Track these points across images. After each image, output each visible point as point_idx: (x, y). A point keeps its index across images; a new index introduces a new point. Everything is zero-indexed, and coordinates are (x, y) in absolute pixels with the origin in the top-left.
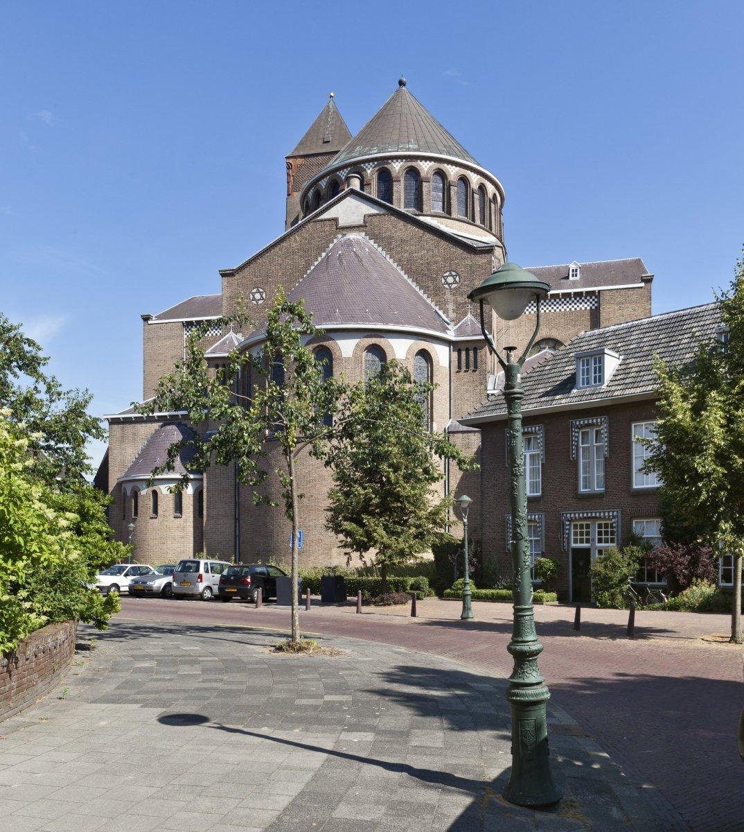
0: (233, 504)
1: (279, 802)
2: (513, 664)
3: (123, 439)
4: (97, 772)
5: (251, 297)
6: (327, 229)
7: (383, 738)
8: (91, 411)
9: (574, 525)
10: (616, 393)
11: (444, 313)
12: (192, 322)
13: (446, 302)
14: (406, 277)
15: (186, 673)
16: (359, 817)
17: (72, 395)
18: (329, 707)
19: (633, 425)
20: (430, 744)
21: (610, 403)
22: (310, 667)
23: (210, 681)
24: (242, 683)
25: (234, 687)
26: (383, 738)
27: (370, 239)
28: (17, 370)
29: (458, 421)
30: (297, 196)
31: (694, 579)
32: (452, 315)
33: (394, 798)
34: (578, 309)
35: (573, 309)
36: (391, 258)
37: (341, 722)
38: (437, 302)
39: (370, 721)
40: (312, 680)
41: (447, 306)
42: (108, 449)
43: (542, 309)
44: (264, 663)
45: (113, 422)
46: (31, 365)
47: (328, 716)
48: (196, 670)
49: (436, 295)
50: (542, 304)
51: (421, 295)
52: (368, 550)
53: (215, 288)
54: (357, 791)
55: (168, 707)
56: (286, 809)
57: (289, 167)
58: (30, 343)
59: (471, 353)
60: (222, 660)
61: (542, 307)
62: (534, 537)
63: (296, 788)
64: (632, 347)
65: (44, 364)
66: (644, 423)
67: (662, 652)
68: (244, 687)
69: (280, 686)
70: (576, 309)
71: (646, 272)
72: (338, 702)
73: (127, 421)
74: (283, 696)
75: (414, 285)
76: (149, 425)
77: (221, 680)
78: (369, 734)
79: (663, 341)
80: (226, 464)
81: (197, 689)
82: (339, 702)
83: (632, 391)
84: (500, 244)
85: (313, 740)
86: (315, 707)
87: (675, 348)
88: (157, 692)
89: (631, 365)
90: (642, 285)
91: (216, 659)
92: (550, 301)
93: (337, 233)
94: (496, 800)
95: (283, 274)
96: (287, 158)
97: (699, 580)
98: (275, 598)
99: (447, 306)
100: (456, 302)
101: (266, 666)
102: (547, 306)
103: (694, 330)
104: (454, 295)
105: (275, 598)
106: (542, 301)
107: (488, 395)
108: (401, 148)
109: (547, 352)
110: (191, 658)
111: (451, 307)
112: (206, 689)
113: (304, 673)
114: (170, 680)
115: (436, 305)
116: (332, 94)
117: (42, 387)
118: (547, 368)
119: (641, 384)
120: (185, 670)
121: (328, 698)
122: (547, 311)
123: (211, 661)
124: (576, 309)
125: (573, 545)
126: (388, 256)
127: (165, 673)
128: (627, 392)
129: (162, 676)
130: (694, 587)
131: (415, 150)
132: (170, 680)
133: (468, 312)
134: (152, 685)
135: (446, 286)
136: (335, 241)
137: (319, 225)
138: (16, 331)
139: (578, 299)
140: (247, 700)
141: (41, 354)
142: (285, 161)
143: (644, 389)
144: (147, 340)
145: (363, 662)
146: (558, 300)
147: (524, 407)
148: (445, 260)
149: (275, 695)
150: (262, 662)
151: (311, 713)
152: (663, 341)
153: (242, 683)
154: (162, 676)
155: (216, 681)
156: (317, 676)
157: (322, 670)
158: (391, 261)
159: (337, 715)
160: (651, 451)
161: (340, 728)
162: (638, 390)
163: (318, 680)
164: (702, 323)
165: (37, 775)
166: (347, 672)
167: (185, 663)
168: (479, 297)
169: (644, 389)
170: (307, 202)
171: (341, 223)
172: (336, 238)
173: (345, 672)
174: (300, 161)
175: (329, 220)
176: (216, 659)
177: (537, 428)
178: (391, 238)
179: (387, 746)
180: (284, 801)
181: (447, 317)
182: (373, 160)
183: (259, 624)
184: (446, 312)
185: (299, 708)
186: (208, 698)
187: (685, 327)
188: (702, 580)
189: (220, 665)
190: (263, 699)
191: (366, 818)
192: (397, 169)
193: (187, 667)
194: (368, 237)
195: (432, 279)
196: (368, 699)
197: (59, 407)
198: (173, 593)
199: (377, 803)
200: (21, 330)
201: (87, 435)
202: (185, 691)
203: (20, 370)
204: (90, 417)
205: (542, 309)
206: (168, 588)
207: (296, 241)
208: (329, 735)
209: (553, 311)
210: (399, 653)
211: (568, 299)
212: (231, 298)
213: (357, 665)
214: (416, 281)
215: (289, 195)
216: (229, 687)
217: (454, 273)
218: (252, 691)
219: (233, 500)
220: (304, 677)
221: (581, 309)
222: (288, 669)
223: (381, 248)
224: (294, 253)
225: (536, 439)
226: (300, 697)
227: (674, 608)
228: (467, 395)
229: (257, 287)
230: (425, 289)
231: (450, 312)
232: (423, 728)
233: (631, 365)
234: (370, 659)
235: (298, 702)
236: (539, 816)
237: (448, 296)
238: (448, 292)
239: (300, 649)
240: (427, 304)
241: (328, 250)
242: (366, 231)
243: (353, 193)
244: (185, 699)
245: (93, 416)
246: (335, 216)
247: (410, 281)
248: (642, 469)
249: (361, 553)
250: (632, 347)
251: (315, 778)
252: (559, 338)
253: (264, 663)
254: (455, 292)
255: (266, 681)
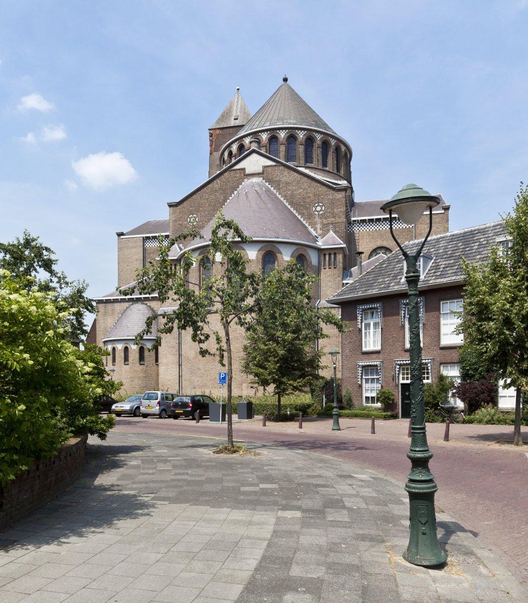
0: (178, 355)
1: (250, 564)
2: (411, 466)
3: (105, 314)
4: (117, 542)
5: (189, 220)
6: (237, 175)
7: (307, 515)
8: (87, 295)
9: (402, 368)
10: (431, 282)
11: (314, 230)
12: (149, 237)
13: (316, 223)
14: (289, 207)
15: (162, 468)
16: (309, 576)
17: (75, 284)
18: (264, 492)
19: (441, 303)
20: (341, 520)
21: (426, 289)
22: (244, 464)
23: (180, 474)
24: (200, 476)
25: (197, 479)
26: (307, 515)
27: (266, 182)
28: (38, 268)
29: (326, 301)
30: (217, 155)
31: (483, 403)
32: (320, 232)
33: (329, 560)
34: (401, 228)
35: (398, 228)
36: (279, 194)
37: (275, 503)
38: (310, 223)
39: (295, 503)
40: (247, 473)
41: (316, 226)
42: (95, 320)
43: (394, 226)
44: (212, 462)
45: (99, 302)
46: (48, 265)
47: (265, 499)
48: (168, 467)
49: (309, 218)
50: (394, 223)
51: (300, 218)
52: (269, 385)
53: (164, 214)
54: (300, 556)
55: (156, 493)
56: (256, 570)
57: (211, 135)
58: (47, 249)
59: (332, 256)
60: (185, 460)
61: (394, 225)
62: (371, 376)
63: (258, 553)
64: (440, 251)
65: (54, 264)
66: (456, 301)
67: (472, 452)
68: (203, 478)
69: (228, 478)
70: (399, 228)
71: (444, 203)
72: (269, 489)
73: (108, 302)
74: (231, 485)
75: (294, 212)
76: (122, 304)
77: (187, 474)
78: (297, 512)
79: (461, 247)
80: (151, 332)
81: (173, 480)
82: (271, 489)
83: (442, 280)
84: (349, 186)
85: (260, 516)
86: (255, 493)
87: (469, 252)
88: (146, 483)
89: (440, 263)
90: (443, 211)
91: (180, 458)
92: (383, 222)
93: (244, 179)
94: (400, 561)
95: (209, 205)
96: (210, 130)
97: (486, 404)
98: (208, 417)
99: (316, 226)
100: (322, 223)
101: (214, 464)
102: (381, 226)
103: (481, 240)
104: (321, 218)
105: (208, 417)
106: (394, 221)
107: (343, 284)
108: (285, 123)
109: (382, 256)
110: (163, 458)
111: (319, 226)
112: (179, 480)
113: (242, 468)
114: (153, 474)
115: (309, 225)
116: (238, 88)
117: (55, 280)
118: (384, 266)
119: (448, 276)
120: (161, 466)
121: (262, 486)
122: (381, 229)
123: (177, 460)
124: (399, 228)
125: (402, 382)
126: (278, 193)
127: (148, 468)
128: (438, 281)
129: (146, 471)
130: (483, 409)
131: (294, 124)
132: (153, 474)
133: (330, 230)
134: (141, 477)
135: (316, 213)
136: (243, 183)
137: (232, 173)
138: (36, 242)
139: (378, 223)
140: (208, 487)
141: (53, 257)
142: (208, 131)
143: (449, 279)
144: (120, 249)
145: (278, 460)
146: (365, 224)
147: (369, 291)
148: (315, 195)
149: (226, 484)
150: (210, 460)
151: (253, 497)
152: (461, 247)
153: (200, 476)
154: (146, 471)
155: (183, 474)
156: (251, 470)
157: (252, 466)
158: (280, 196)
159: (272, 498)
160: (461, 320)
161: (276, 508)
162: (446, 279)
163: (252, 473)
164: (487, 236)
165: (77, 545)
166: (270, 467)
167: (159, 461)
168: (388, 209)
169: (449, 279)
170: (224, 159)
171: (247, 172)
172: (243, 181)
173: (268, 467)
174: (218, 132)
175: (239, 169)
176: (180, 458)
177: (378, 305)
178: (280, 181)
179: (312, 521)
180: (253, 563)
181: (317, 233)
182: (266, 130)
183: (200, 434)
184: (315, 230)
185: (244, 493)
186: (182, 487)
187: (475, 238)
188: (488, 404)
189: (183, 463)
190: (219, 487)
191: (314, 576)
192: (283, 136)
193: (162, 465)
194: (264, 181)
195: (307, 208)
196: (289, 487)
197: (67, 292)
198: (140, 413)
199: (318, 565)
200: (39, 241)
201: (85, 310)
202: (165, 482)
203: (40, 267)
204: (87, 298)
205: (394, 226)
206: (137, 411)
207: (217, 184)
208: (270, 513)
209: (384, 229)
210: (299, 454)
211: (365, 224)
212: (175, 221)
213: (275, 463)
214: (296, 209)
215: (210, 154)
216: (193, 478)
217: (316, 205)
218: (210, 481)
219: (178, 354)
220: (242, 471)
221: (403, 227)
222: (228, 466)
223: (273, 188)
224: (216, 191)
225: (377, 312)
226: (243, 485)
227: (470, 422)
228: (330, 284)
229: (193, 214)
230: (302, 215)
231: (319, 230)
232: (332, 508)
233: (440, 263)
234: (282, 458)
235: (242, 489)
236: (432, 572)
237: (317, 219)
238: (317, 216)
239: (235, 452)
240: (304, 225)
241: (238, 189)
242: (263, 177)
243: (254, 151)
244: (166, 487)
245: (89, 298)
246: (243, 167)
247: (292, 209)
248: (454, 331)
249: (264, 387)
250: (440, 251)
251: (269, 546)
252: (388, 246)
253: (212, 462)
254: (321, 217)
255: (216, 474)
